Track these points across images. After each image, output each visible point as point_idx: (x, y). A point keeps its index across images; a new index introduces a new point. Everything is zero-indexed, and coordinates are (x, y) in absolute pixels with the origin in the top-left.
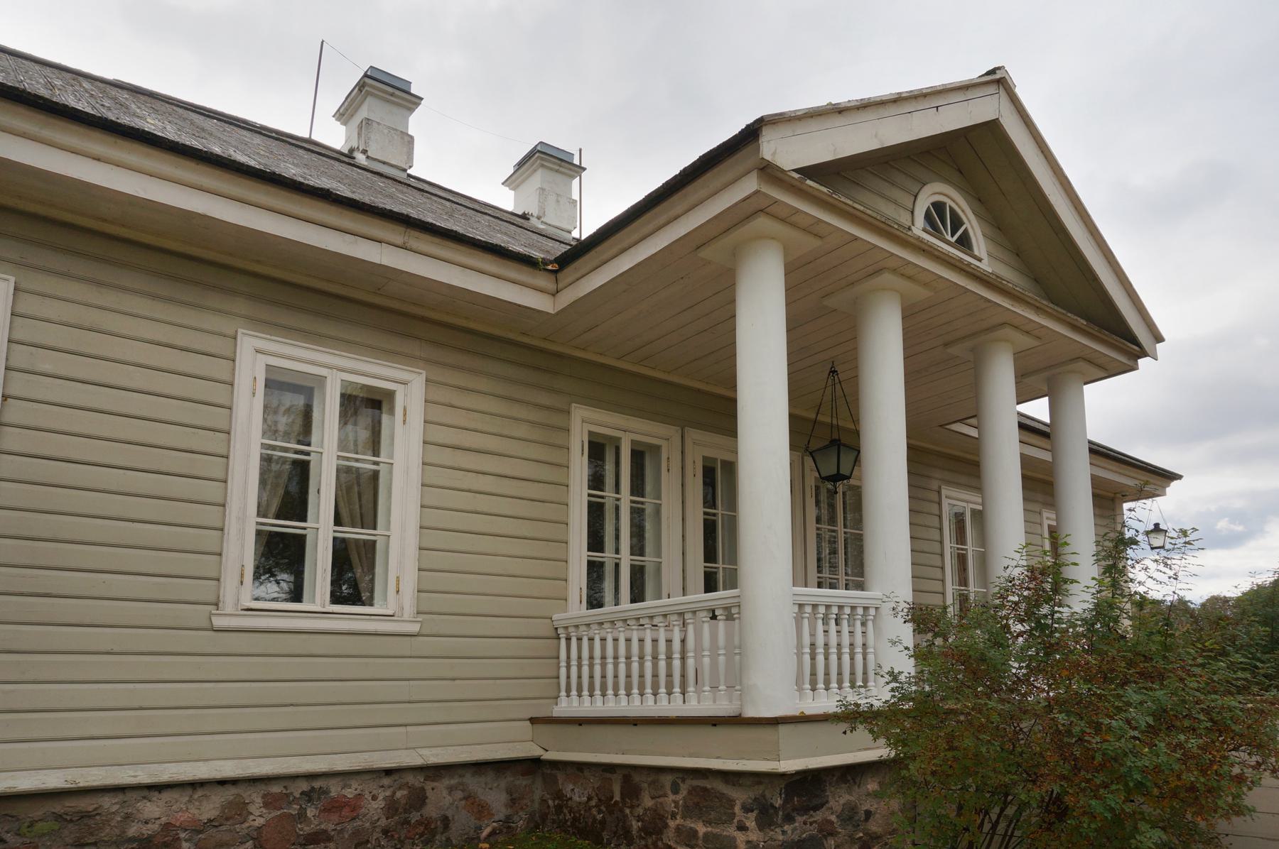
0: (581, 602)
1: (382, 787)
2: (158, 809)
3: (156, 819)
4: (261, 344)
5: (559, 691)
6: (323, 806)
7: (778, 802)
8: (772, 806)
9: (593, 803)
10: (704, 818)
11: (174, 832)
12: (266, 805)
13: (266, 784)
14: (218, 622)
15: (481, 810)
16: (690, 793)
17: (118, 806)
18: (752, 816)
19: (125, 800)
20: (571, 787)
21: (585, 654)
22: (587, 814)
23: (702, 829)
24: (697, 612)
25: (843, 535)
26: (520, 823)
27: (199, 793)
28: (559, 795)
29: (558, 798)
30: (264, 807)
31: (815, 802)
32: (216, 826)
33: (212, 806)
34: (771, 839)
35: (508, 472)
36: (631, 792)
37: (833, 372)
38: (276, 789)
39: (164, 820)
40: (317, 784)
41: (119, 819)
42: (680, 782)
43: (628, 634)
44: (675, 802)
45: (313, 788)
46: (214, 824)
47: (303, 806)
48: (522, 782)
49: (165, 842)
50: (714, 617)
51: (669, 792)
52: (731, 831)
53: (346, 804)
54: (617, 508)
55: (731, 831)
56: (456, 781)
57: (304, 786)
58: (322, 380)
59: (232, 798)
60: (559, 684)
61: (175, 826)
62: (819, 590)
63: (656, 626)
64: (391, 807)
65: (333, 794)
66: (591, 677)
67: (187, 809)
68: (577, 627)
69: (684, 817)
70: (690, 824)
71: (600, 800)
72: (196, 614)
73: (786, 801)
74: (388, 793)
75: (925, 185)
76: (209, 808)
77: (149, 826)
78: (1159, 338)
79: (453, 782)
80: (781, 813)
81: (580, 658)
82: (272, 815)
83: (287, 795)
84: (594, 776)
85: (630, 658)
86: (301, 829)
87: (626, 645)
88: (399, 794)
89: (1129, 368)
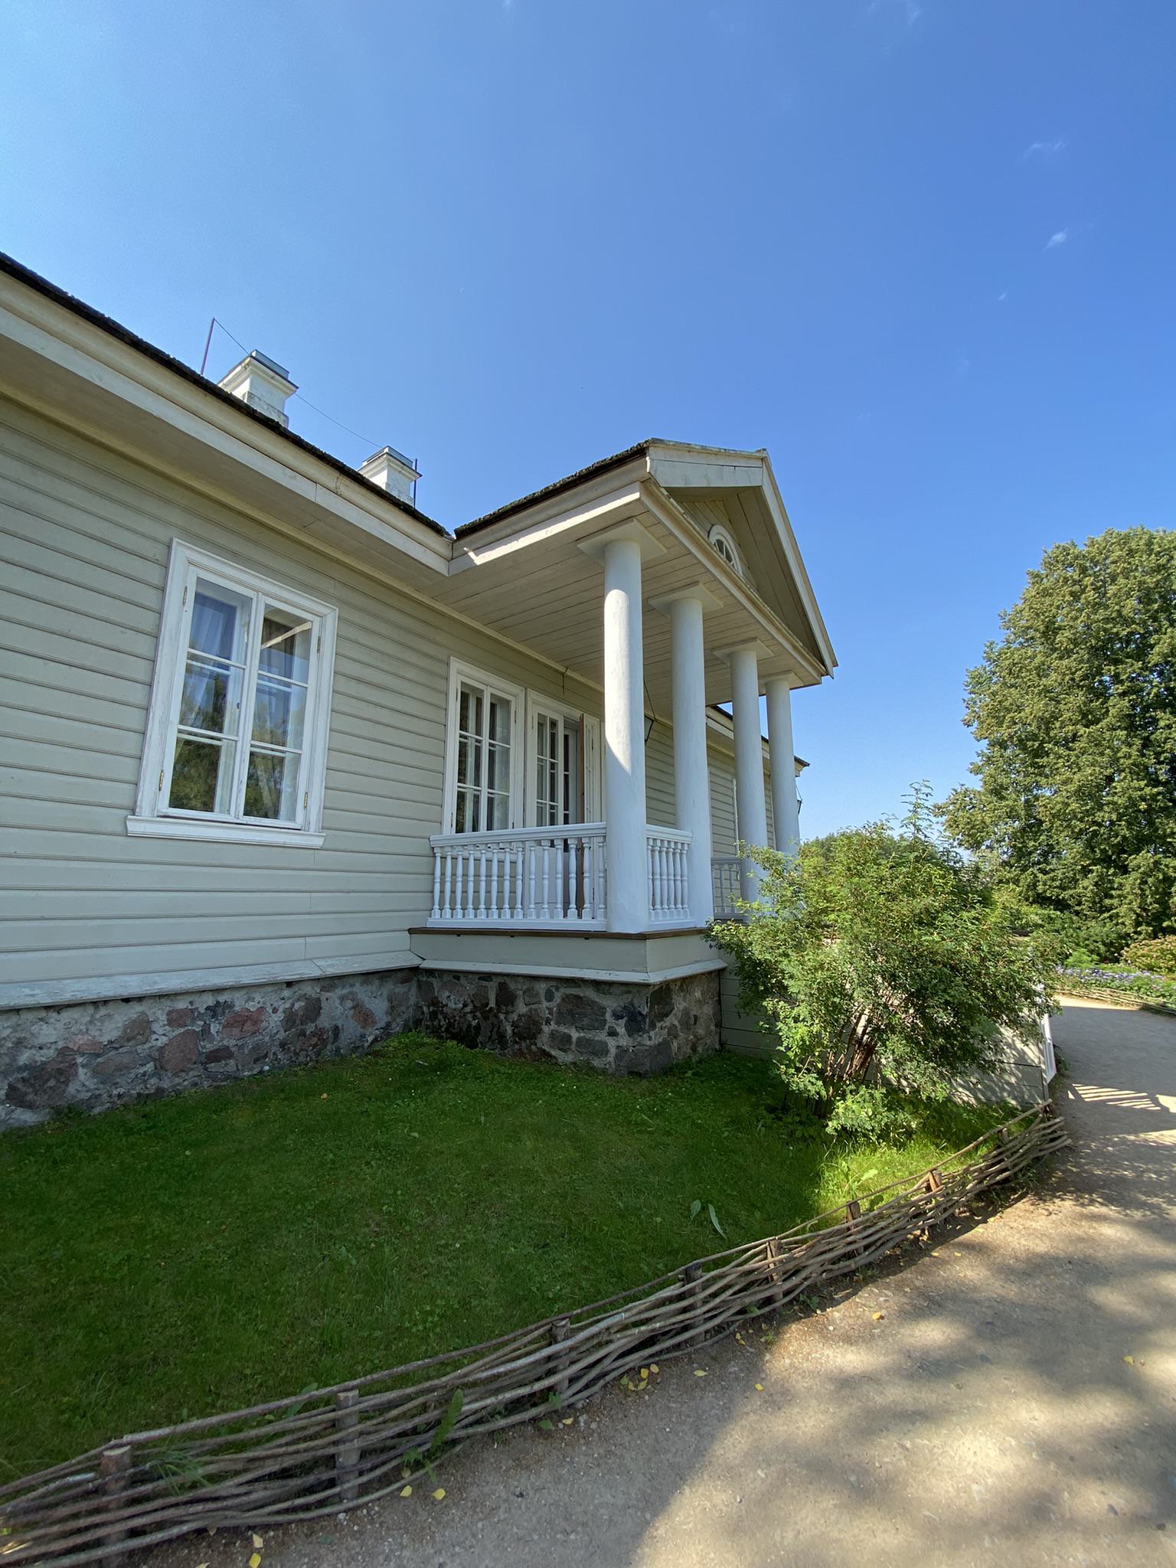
1: (283, 999)
2: (54, 1032)
3: (51, 1043)
4: (195, 557)
5: (433, 904)
6: (226, 1021)
7: (645, 1011)
8: (640, 1013)
9: (468, 1009)
10: (577, 1024)
11: (71, 1057)
12: (171, 1022)
13: (172, 1000)
14: (134, 827)
15: (365, 1017)
16: (563, 1000)
17: (10, 1030)
18: (622, 1022)
19: (20, 1022)
20: (447, 994)
21: (460, 871)
22: (462, 1020)
23: (575, 1035)
25: (488, 747)
26: (396, 1028)
27: (103, 1011)
28: (435, 1002)
29: (433, 1005)
30: (169, 1025)
31: (668, 1008)
32: (117, 1049)
33: (114, 1026)
34: (640, 1044)
35: (399, 708)
36: (506, 998)
38: (182, 1004)
39: (61, 1045)
40: (222, 999)
41: (10, 1045)
44: (549, 1009)
45: (218, 1002)
46: (115, 1045)
47: (208, 1022)
48: (400, 989)
49: (60, 1069)
50: (552, 845)
51: (543, 999)
52: (602, 1036)
53: (249, 1018)
55: (602, 1036)
56: (348, 990)
57: (209, 1000)
58: (246, 601)
59: (136, 1016)
60: (433, 897)
61: (72, 1050)
64: (290, 1019)
65: (237, 1008)
66: (453, 892)
67: (87, 1030)
69: (558, 1023)
70: (563, 1029)
71: (474, 1006)
72: (110, 819)
73: (651, 1008)
74: (288, 1005)
76: (111, 1027)
77: (45, 1051)
78: (835, 665)
79: (345, 991)
82: (177, 1032)
83: (192, 1011)
84: (471, 983)
85: (491, 876)
86: (204, 1047)
88: (297, 1006)
89: (816, 682)
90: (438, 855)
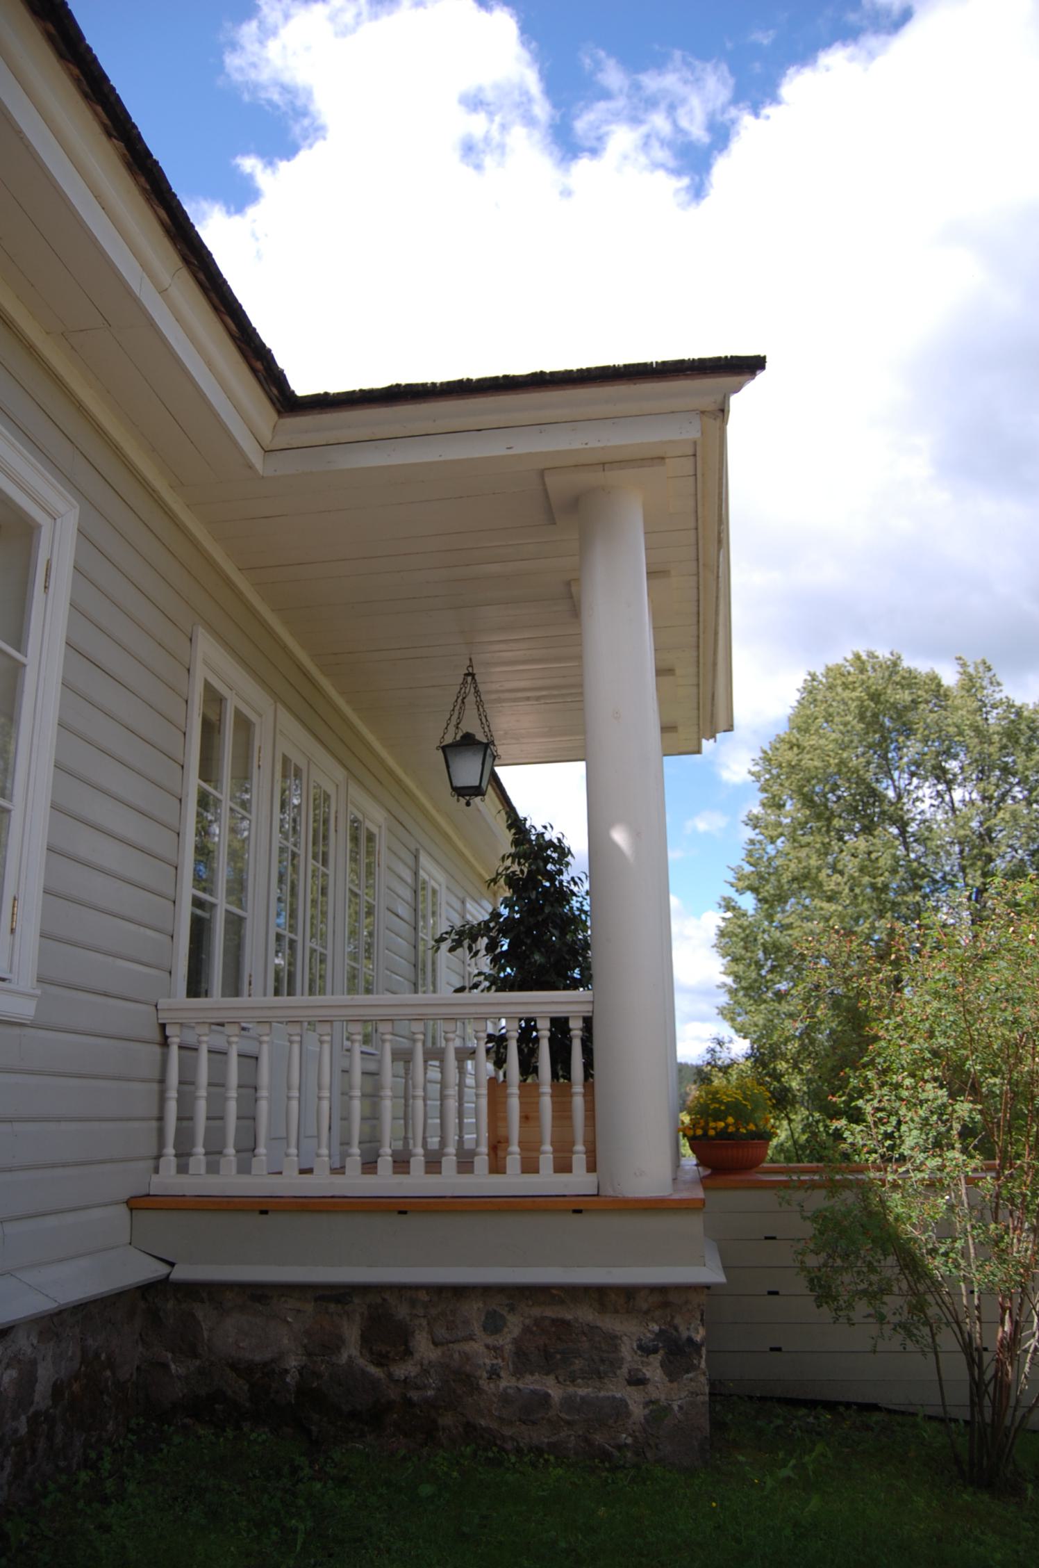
8: (690, 1340)
16: (526, 1330)
18: (656, 1359)
42: (504, 1313)
55: (617, 1390)
62: (276, 998)
80: (704, 1350)
90: (174, 1041)
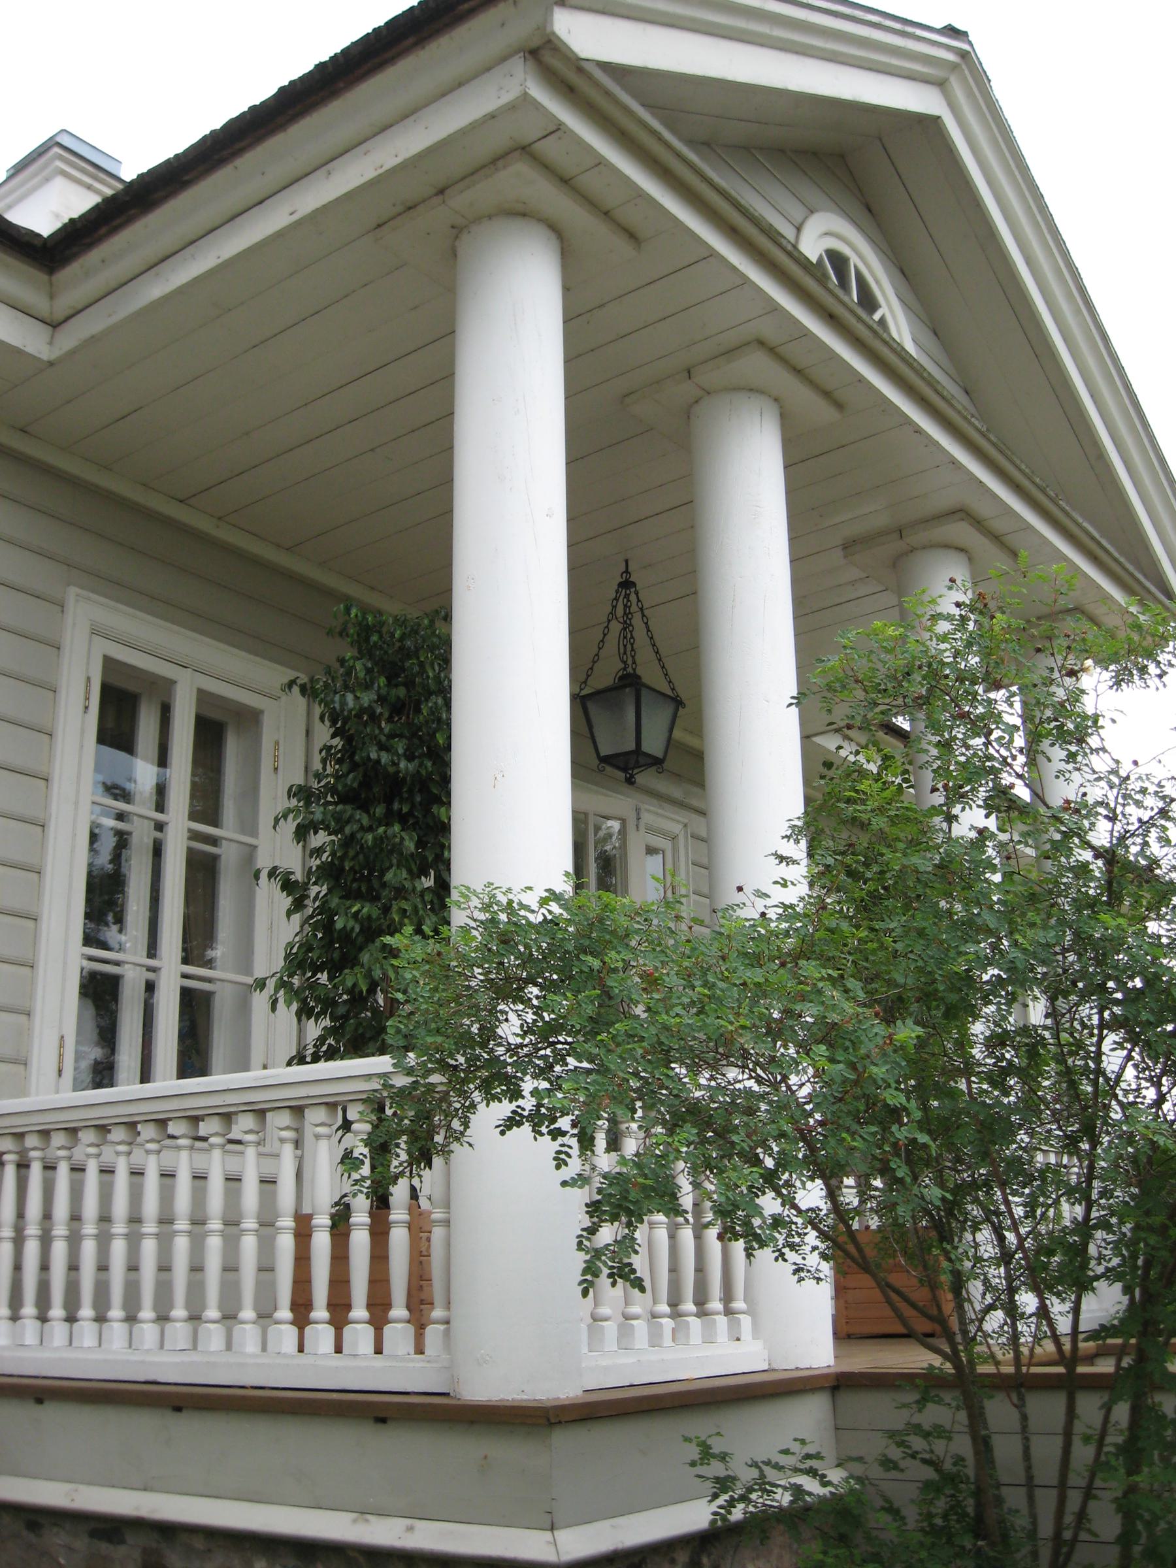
0: (60, 1072)
21: (61, 1209)
24: (269, 1115)
37: (627, 584)
43: (200, 1161)
54: (158, 851)
63: (239, 1142)
68: (45, 1134)
75: (812, 212)
81: (47, 1216)
87: (262, 1195)
